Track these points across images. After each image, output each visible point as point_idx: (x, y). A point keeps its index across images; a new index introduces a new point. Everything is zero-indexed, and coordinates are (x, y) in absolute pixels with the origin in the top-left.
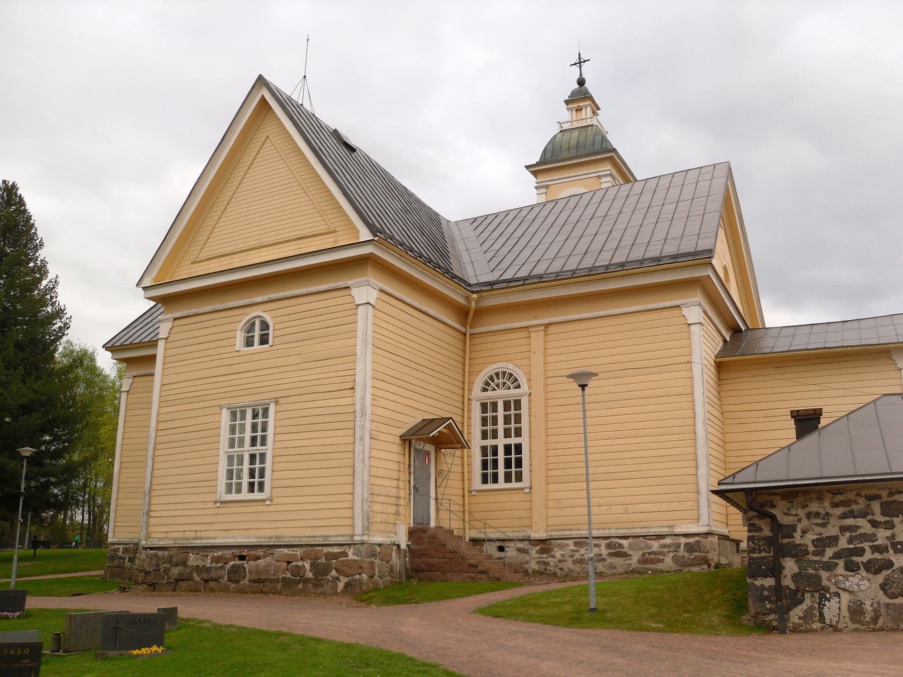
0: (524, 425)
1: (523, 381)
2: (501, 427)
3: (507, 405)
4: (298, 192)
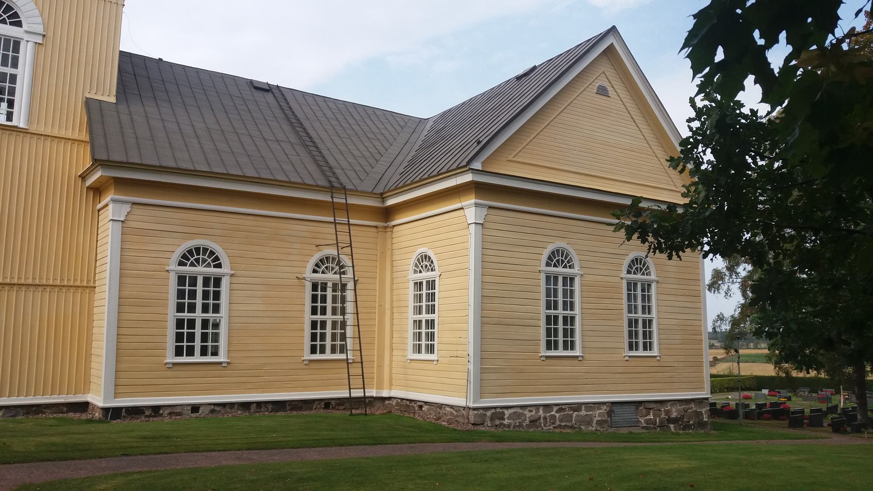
0: (224, 301)
1: (224, 260)
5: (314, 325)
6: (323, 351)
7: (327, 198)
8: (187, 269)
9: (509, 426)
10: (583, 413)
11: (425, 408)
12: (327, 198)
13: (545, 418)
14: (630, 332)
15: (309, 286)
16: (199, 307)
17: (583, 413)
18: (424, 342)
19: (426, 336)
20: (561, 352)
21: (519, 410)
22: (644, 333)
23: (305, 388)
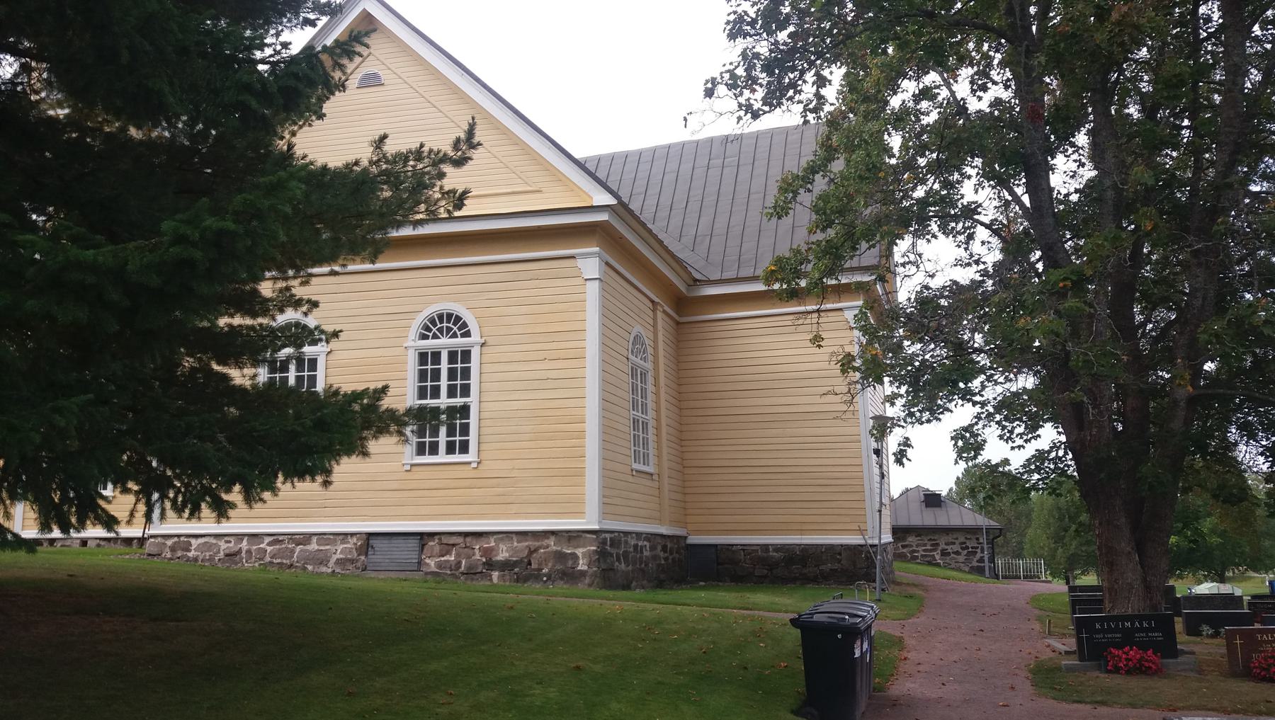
0: (474, 381)
1: (473, 326)
2: (444, 383)
3: (452, 356)
4: (619, 393)
8: (430, 343)
9: (196, 559)
10: (313, 546)
13: (249, 552)
17: (313, 546)
21: (213, 541)
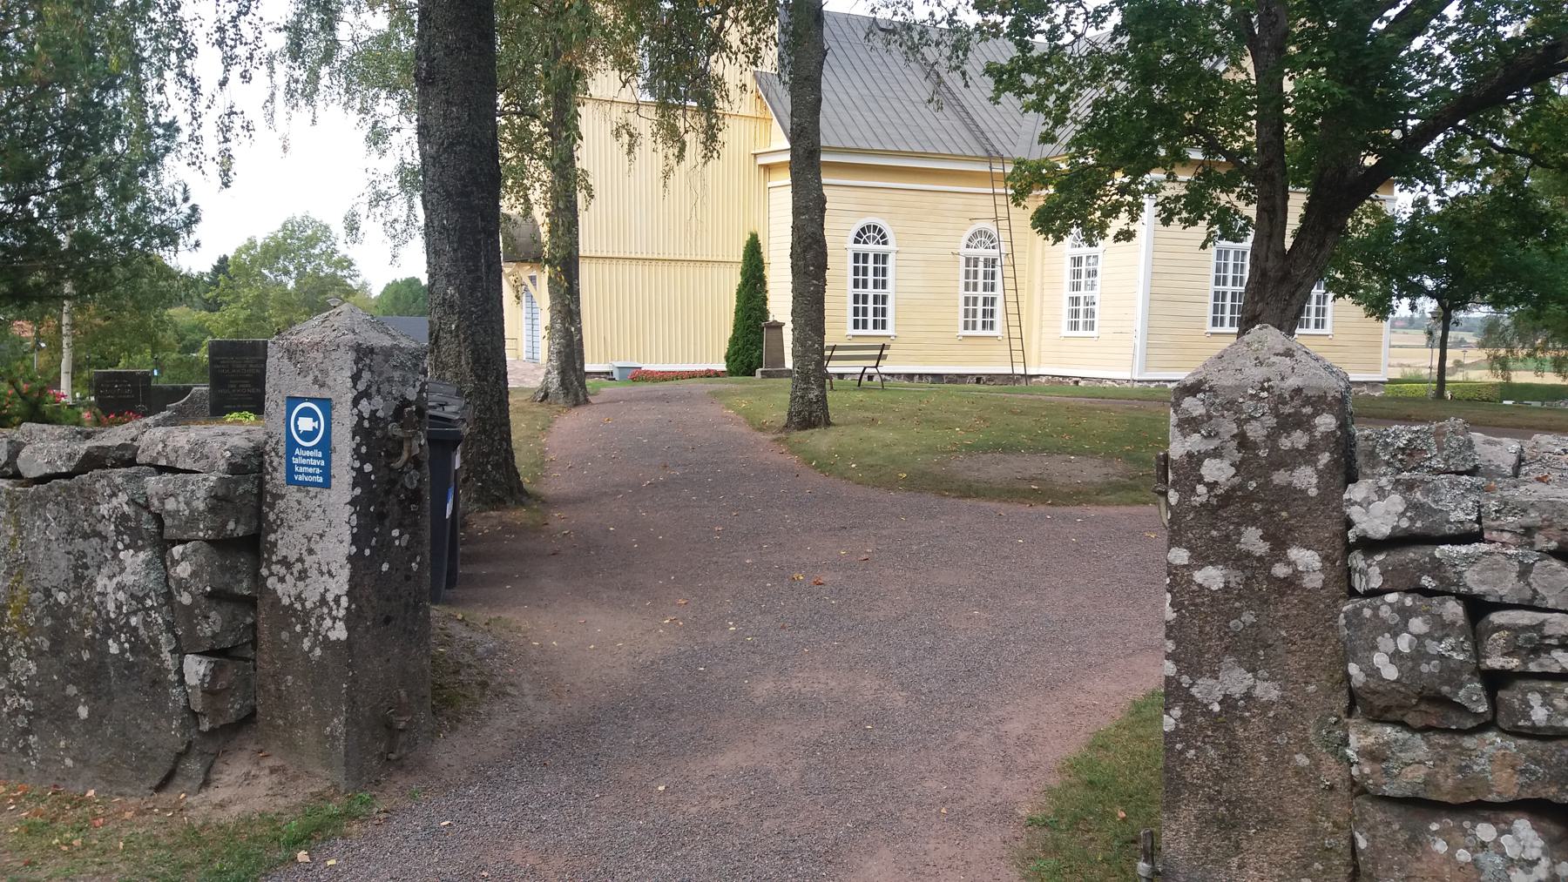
1: (889, 238)
5: (856, 298)
6: (865, 327)
7: (985, 168)
8: (861, 247)
11: (1082, 383)
12: (985, 168)
14: (1216, 306)
15: (963, 260)
16: (870, 284)
18: (1081, 319)
19: (1082, 315)
20: (979, 331)
22: (1318, 310)
23: (961, 362)
